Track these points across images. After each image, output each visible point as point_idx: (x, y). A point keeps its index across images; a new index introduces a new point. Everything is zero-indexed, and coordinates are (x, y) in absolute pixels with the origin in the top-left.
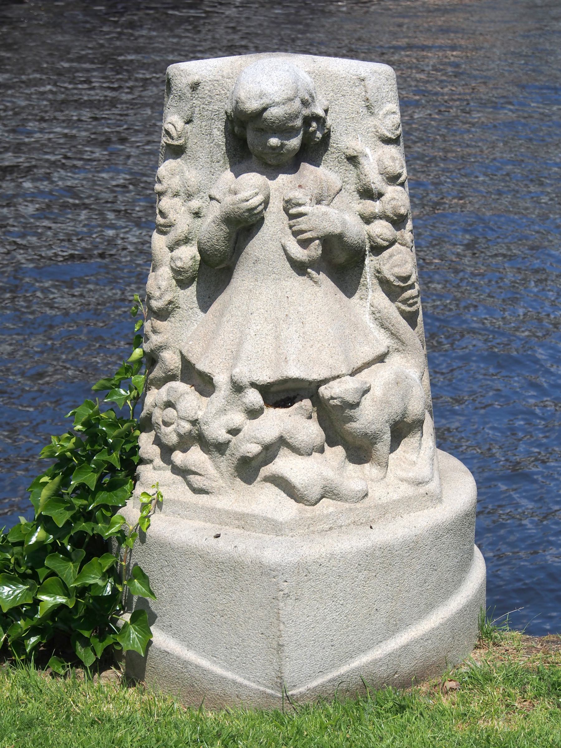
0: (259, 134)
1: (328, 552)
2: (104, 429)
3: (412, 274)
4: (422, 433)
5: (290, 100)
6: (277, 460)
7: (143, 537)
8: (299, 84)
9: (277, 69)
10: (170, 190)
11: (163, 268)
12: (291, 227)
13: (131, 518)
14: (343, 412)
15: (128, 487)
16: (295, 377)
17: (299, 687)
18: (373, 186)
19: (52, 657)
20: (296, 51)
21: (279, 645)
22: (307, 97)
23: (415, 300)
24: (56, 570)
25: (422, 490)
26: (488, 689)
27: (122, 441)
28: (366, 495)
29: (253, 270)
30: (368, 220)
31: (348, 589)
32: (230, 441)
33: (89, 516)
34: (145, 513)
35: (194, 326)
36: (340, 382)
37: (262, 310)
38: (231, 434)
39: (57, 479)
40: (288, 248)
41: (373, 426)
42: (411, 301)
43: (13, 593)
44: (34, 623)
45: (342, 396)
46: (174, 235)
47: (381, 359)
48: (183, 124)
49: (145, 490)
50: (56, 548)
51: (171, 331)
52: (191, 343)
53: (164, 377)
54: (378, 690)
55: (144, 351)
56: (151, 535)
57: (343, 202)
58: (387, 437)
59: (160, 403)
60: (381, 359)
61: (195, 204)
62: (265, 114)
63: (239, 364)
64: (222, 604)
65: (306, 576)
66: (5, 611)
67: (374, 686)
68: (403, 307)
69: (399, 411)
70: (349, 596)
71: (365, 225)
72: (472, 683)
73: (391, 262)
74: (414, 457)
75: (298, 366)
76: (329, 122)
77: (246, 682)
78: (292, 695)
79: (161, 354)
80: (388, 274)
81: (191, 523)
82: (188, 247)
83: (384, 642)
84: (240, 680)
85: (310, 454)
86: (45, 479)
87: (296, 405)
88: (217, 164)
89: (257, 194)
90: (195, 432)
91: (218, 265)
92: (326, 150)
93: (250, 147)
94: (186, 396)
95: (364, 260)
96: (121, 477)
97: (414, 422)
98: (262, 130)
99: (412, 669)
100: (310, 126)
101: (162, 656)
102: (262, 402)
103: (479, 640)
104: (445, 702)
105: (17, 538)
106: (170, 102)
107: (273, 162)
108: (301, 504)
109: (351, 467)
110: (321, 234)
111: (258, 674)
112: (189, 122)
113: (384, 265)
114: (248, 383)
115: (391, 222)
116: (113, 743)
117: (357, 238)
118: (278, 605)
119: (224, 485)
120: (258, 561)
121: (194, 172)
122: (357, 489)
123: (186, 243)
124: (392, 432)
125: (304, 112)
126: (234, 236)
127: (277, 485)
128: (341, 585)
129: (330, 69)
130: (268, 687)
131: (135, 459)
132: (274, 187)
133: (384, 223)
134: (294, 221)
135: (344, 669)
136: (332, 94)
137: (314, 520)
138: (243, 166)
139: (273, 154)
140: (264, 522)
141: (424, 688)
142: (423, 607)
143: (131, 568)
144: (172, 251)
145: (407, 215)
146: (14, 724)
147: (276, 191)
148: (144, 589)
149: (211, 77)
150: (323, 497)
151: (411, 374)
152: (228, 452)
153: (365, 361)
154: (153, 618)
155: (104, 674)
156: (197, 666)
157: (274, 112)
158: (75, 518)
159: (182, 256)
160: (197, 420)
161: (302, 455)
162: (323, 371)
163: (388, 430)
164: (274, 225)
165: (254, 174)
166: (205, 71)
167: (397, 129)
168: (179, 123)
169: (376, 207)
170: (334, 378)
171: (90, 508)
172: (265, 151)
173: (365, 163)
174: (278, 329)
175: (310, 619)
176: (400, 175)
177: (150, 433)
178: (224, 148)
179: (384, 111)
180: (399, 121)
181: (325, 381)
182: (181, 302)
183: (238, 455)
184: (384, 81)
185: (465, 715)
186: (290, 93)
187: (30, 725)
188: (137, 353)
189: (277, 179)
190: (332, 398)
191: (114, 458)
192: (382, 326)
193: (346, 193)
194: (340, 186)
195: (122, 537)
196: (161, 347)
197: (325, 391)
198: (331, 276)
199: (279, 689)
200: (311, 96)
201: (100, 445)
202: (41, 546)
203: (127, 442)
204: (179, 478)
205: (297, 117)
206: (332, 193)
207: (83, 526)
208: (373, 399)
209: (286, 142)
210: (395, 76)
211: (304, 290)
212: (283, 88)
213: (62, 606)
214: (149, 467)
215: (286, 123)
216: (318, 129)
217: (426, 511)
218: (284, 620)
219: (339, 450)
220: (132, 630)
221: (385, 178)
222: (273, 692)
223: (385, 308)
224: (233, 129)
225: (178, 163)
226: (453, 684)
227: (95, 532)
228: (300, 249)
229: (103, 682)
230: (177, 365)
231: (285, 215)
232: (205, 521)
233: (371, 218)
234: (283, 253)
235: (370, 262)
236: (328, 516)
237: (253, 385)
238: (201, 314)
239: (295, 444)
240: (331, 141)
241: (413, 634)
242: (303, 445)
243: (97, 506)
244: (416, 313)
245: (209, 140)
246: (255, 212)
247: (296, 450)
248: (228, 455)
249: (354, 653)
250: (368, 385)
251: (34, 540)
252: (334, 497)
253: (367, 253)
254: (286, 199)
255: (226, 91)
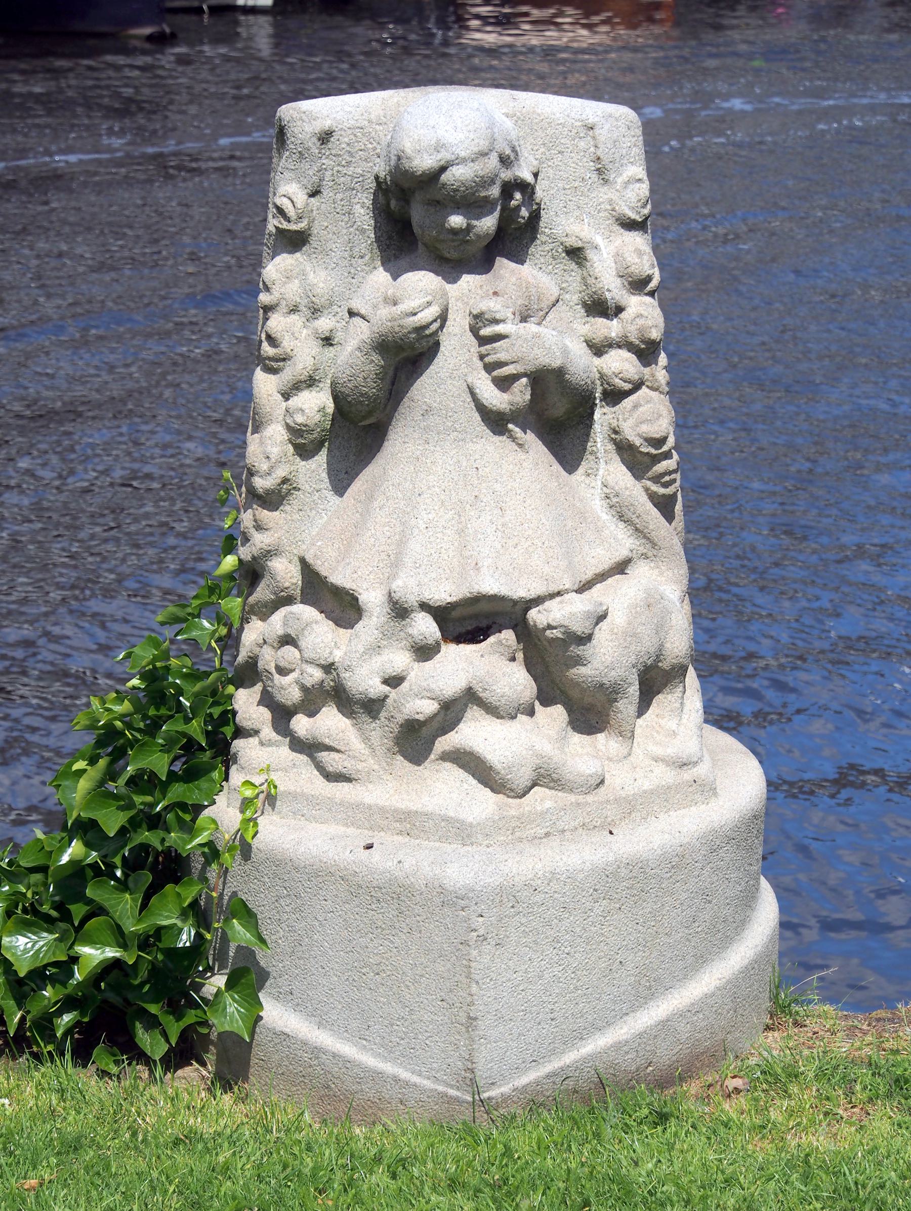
0: (432, 210)
1: (548, 869)
2: (178, 681)
3: (668, 434)
4: (685, 687)
5: (484, 154)
6: (461, 726)
7: (246, 850)
8: (496, 130)
9: (460, 106)
10: (284, 303)
11: (273, 426)
12: (482, 357)
13: (226, 822)
14: (567, 651)
15: (216, 775)
16: (492, 592)
17: (501, 1086)
18: (608, 295)
19: (101, 1045)
20: (484, 84)
21: (470, 1018)
22: (508, 152)
23: (673, 476)
24: (106, 904)
25: (688, 775)
26: (794, 1089)
27: (206, 702)
28: (602, 782)
29: (422, 425)
30: (598, 349)
31: (578, 929)
32: (386, 697)
33: (155, 822)
34: (248, 814)
35: (322, 518)
36: (561, 602)
37: (437, 489)
38: (389, 685)
39: (102, 763)
40: (477, 391)
41: (613, 673)
42: (667, 478)
43: (33, 946)
44: (69, 990)
45: (566, 623)
46: (289, 374)
47: (621, 568)
48: (306, 197)
49: (248, 778)
50: (101, 872)
51: (286, 527)
52: (319, 543)
53: (273, 601)
54: (624, 1090)
55: (240, 560)
56: (260, 847)
57: (561, 319)
58: (634, 690)
59: (272, 637)
60: (621, 568)
61: (324, 324)
62: (444, 177)
63: (401, 574)
64: (377, 954)
65: (513, 907)
66: (22, 974)
67: (617, 1084)
68: (655, 488)
69: (652, 650)
70: (579, 940)
71: (595, 358)
72: (767, 1082)
73: (635, 416)
74: (672, 724)
75: (496, 575)
76: (539, 193)
77: (415, 1079)
78: (489, 1099)
79: (269, 563)
80: (632, 433)
81: (324, 828)
82: (314, 393)
83: (632, 1015)
84: (404, 1075)
85: (513, 717)
86: (80, 765)
87: (492, 639)
88: (360, 261)
89: (429, 304)
90: (329, 683)
91: (364, 418)
92: (534, 238)
93: (416, 230)
94: (314, 626)
95: (593, 413)
96: (204, 759)
97: (673, 667)
98: (438, 202)
99: (674, 1058)
100: (511, 198)
101: (277, 1041)
102: (438, 634)
103: (771, 1018)
104: (729, 1108)
105: (33, 861)
106: (284, 162)
107: (453, 255)
108: (501, 796)
109: (577, 739)
110: (530, 368)
111: (435, 1065)
112: (315, 193)
113: (625, 420)
114: (416, 604)
115: (635, 353)
116: (213, 1170)
117: (584, 376)
118: (469, 954)
119: (376, 767)
120: (436, 884)
121: (323, 274)
122: (588, 772)
123: (310, 386)
124: (641, 683)
125: (503, 175)
126: (391, 372)
127: (462, 766)
128: (566, 923)
129: (539, 111)
130: (452, 1087)
131: (228, 731)
132: (455, 294)
133: (625, 354)
134: (488, 347)
135: (570, 1058)
136: (542, 150)
137: (522, 821)
138: (403, 263)
139: (453, 241)
140: (443, 824)
141: (693, 1088)
142: (690, 960)
143: (225, 902)
144: (287, 399)
145: (659, 343)
146: (50, 1144)
147: (457, 300)
148: (248, 935)
149: (353, 122)
150: (534, 785)
151: (667, 593)
152: (383, 714)
153: (597, 571)
154: (263, 977)
155: (180, 1073)
156: (334, 1055)
157: (458, 174)
158: (134, 824)
159: (304, 407)
160: (333, 664)
161: (502, 718)
162: (534, 585)
163: (634, 679)
164: (455, 354)
165: (423, 272)
166: (341, 113)
167: (644, 206)
168: (299, 196)
169: (612, 328)
170: (552, 596)
171: (158, 809)
172: (441, 237)
173: (595, 258)
174: (463, 518)
175: (518, 977)
176: (649, 279)
177: (252, 689)
178: (373, 236)
179: (624, 177)
180: (647, 193)
181: (537, 601)
182: (302, 480)
183: (400, 719)
184: (623, 130)
185: (764, 1128)
186: (483, 145)
187: (75, 1146)
188: (229, 562)
189: (459, 283)
190: (550, 627)
191: (196, 728)
192: (621, 517)
193: (564, 307)
194: (556, 295)
195: (212, 852)
196: (269, 552)
197: (536, 616)
198: (541, 436)
199: (470, 1089)
200: (514, 150)
201: (170, 710)
202: (78, 870)
203: (215, 704)
204: (303, 758)
205: (493, 182)
206: (545, 305)
207: (145, 836)
208: (612, 630)
209: (475, 223)
210: (640, 124)
211: (502, 458)
212: (472, 136)
213: (116, 964)
214: (253, 741)
215: (476, 191)
216: (523, 203)
217: (693, 809)
218: (477, 977)
219: (558, 712)
220: (229, 1000)
221: (626, 283)
222: (459, 1094)
223: (627, 488)
224: (388, 204)
225: (297, 260)
226: (738, 1083)
227: (167, 844)
228: (496, 392)
229: (180, 1085)
230: (294, 581)
231: (473, 338)
232: (346, 825)
233: (604, 346)
234: (469, 399)
235: (603, 416)
236: (543, 814)
237: (424, 606)
238: (334, 500)
239: (491, 700)
240: (541, 224)
241: (676, 1002)
242: (503, 701)
243: (167, 806)
244: (672, 498)
245: (347, 223)
246: (427, 332)
247: (492, 710)
248: (383, 719)
249: (585, 1032)
250: (605, 608)
251: (65, 859)
252: (552, 784)
253: (598, 401)
254: (475, 312)
255: (375, 144)
